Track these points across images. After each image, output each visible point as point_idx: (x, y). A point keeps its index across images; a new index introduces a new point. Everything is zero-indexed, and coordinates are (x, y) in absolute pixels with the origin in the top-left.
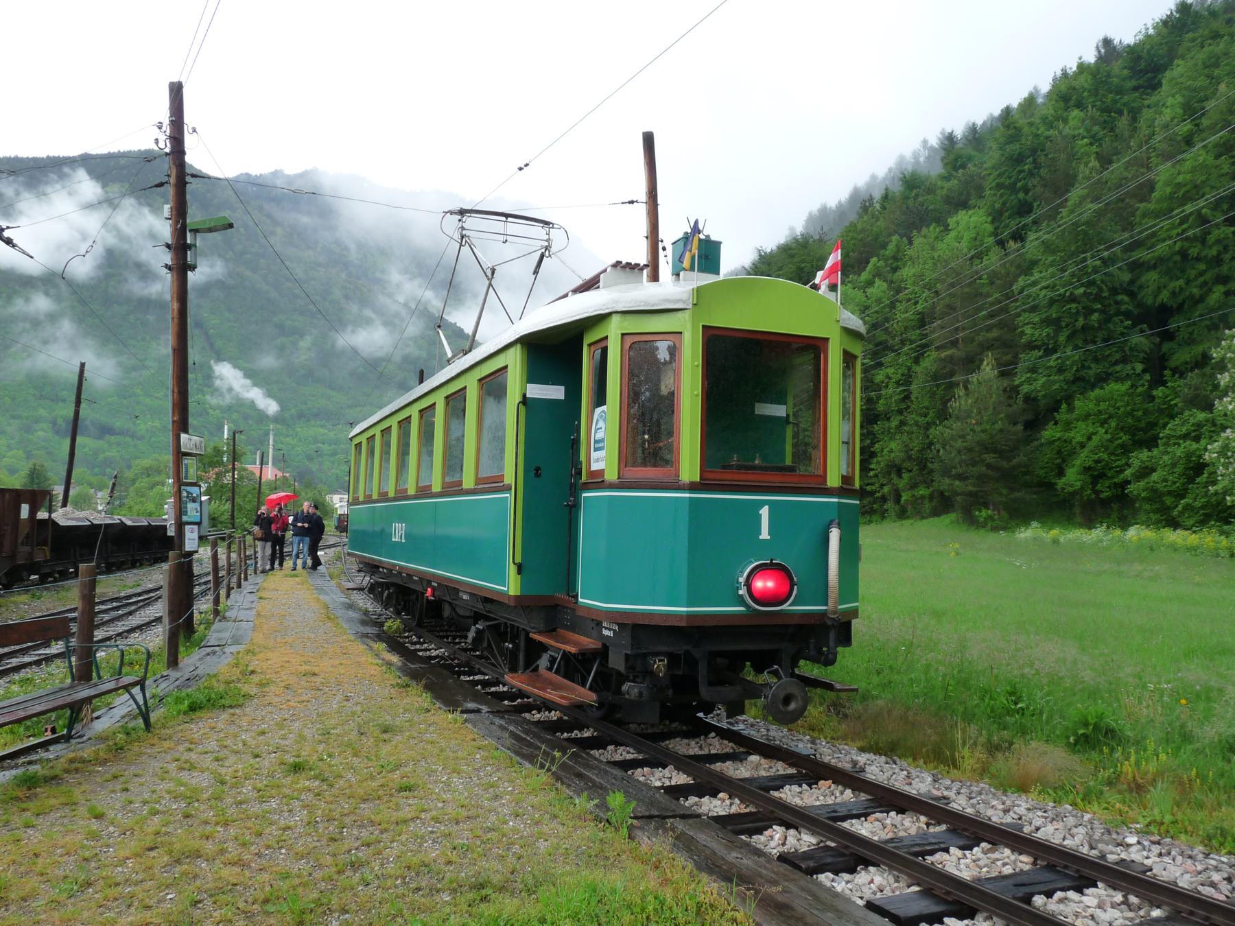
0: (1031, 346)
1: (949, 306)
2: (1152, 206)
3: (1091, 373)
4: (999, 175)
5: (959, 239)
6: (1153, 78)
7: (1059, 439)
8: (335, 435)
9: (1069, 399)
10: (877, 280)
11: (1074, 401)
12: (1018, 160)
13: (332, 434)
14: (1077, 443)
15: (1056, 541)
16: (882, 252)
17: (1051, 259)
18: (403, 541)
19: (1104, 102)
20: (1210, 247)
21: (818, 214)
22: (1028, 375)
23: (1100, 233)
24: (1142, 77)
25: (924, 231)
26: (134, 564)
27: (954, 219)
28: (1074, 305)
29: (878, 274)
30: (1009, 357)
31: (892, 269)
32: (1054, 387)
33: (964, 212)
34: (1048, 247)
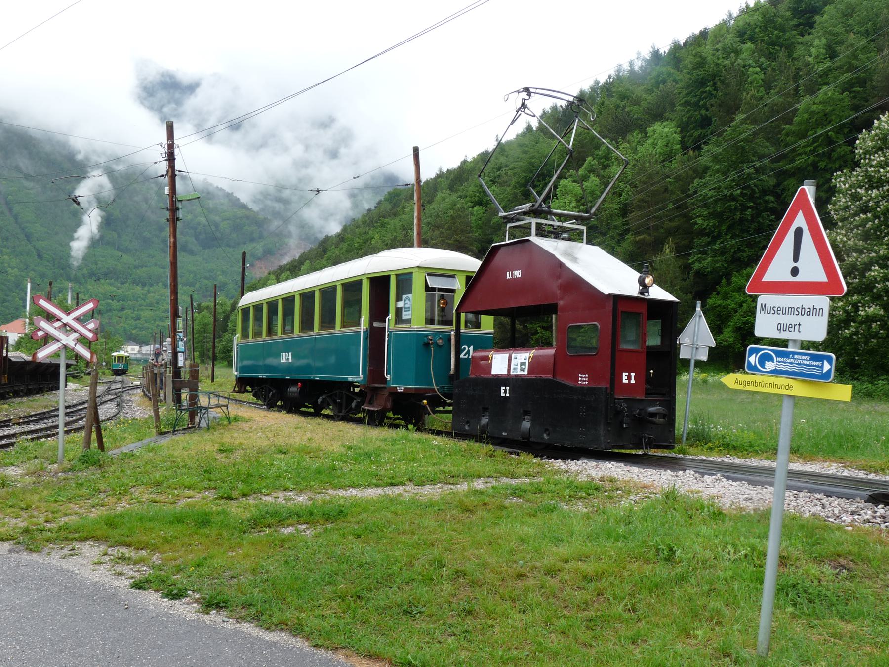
0: (702, 233)
1: (643, 200)
2: (793, 128)
3: (744, 254)
4: (687, 94)
5: (654, 145)
6: (810, 18)
7: (719, 306)
8: (123, 292)
9: (728, 276)
10: (592, 176)
11: (732, 276)
12: (702, 83)
13: (120, 291)
14: (732, 309)
15: (705, 382)
16: (596, 152)
17: (718, 167)
18: (633, 382)
19: (770, 37)
20: (834, 161)
21: (550, 111)
22: (699, 256)
23: (754, 148)
24: (803, 16)
25: (629, 137)
26: (29, 393)
27: (652, 129)
28: (733, 203)
29: (591, 171)
30: (686, 242)
31: (604, 166)
32: (717, 265)
33: (659, 123)
34: (716, 159)
